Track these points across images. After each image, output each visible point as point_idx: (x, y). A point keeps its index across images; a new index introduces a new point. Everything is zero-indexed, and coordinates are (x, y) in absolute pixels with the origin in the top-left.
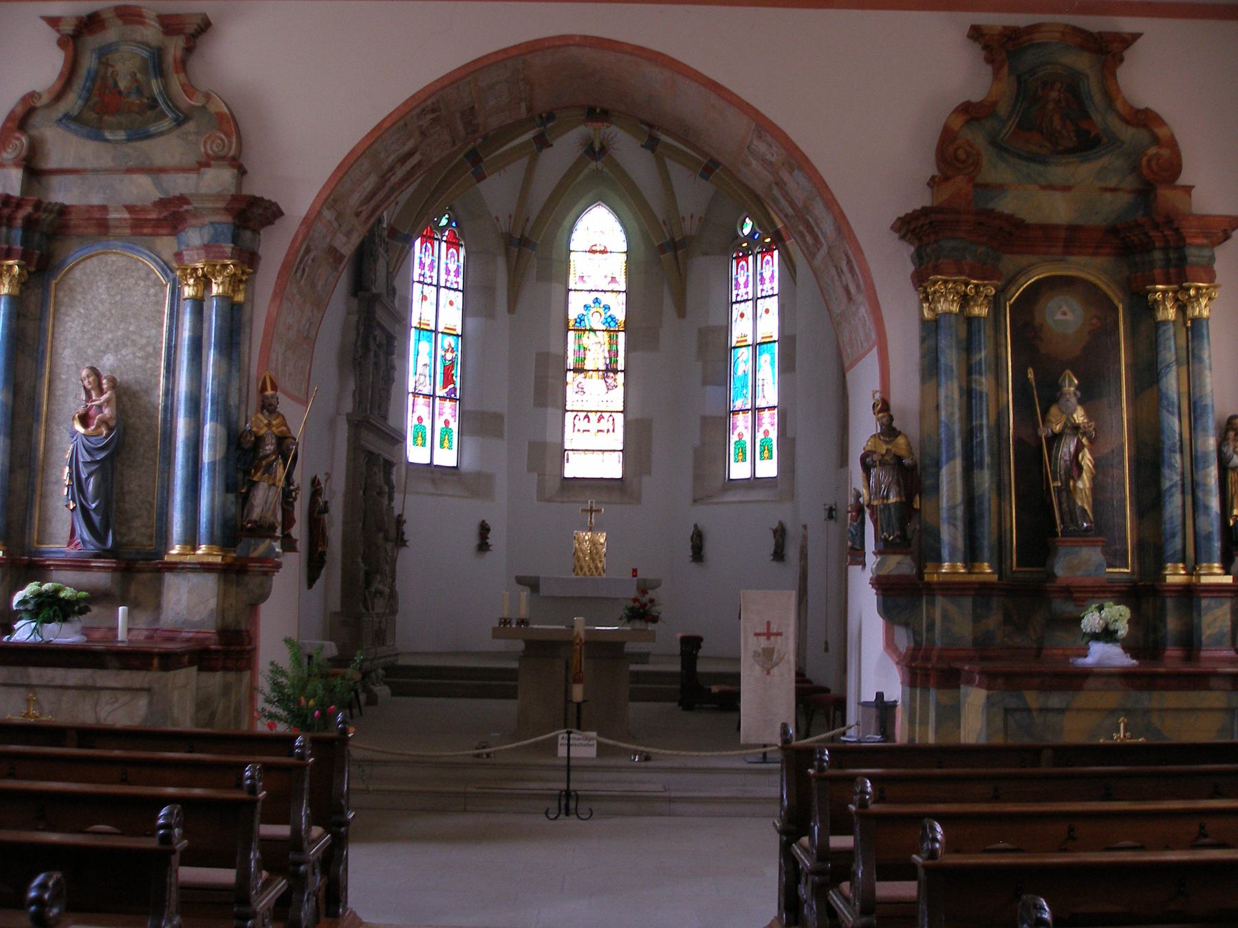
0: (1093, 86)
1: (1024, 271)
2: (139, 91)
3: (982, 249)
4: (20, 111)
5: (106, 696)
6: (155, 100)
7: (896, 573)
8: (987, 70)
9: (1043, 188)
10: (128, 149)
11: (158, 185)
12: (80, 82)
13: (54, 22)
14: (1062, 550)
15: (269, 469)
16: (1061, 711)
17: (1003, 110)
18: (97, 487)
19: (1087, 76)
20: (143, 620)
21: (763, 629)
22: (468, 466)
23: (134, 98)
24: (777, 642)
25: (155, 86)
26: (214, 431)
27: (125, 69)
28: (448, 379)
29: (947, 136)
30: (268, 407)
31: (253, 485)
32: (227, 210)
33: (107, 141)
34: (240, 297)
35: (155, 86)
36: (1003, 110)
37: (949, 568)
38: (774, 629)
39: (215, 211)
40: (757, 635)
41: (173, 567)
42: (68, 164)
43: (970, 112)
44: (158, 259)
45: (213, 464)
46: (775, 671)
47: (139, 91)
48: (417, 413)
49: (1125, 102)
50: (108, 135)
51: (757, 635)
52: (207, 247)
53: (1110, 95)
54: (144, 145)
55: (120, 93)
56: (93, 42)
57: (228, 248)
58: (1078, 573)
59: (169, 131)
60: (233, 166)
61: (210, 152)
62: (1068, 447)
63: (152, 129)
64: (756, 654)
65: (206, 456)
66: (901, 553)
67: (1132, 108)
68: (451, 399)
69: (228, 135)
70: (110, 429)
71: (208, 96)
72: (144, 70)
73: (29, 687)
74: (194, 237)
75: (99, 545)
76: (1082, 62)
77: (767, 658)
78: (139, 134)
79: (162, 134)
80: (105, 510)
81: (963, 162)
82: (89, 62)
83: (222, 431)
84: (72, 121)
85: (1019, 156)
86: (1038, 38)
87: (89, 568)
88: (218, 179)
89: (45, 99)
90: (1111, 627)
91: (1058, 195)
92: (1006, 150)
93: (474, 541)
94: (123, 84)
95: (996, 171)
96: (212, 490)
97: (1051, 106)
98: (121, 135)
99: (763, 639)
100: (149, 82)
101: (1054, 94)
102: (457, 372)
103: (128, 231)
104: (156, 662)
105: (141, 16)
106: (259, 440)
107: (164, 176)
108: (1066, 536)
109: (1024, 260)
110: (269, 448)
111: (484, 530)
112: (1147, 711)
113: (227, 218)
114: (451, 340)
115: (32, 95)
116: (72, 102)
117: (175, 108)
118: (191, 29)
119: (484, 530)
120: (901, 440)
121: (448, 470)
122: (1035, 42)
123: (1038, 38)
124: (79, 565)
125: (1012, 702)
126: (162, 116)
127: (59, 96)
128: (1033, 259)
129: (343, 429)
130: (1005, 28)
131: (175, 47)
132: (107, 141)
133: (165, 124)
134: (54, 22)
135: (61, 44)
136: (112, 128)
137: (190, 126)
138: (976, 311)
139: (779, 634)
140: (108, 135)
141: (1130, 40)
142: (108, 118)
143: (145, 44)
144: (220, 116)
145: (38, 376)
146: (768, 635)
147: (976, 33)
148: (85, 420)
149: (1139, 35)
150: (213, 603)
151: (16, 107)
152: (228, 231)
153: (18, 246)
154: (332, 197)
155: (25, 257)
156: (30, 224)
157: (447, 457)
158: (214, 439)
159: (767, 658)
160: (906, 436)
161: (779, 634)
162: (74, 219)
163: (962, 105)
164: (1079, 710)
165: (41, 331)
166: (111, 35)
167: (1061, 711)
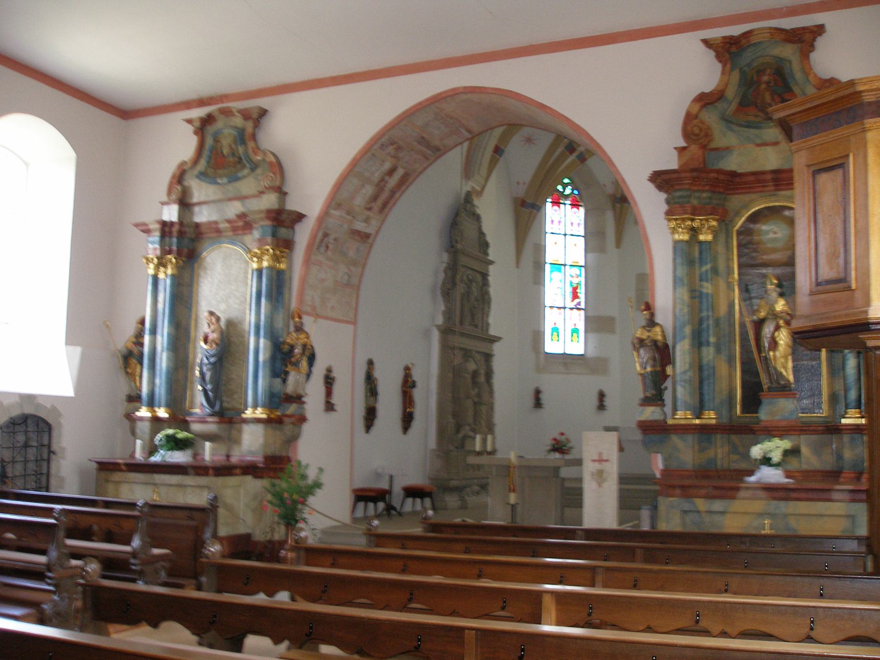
0: (796, 67)
1: (746, 207)
2: (233, 155)
3: (705, 195)
4: (178, 173)
5: (189, 490)
6: (240, 158)
7: (651, 418)
8: (719, 67)
9: (758, 145)
10: (230, 187)
11: (243, 205)
12: (206, 153)
13: (189, 121)
14: (765, 401)
15: (296, 364)
16: (722, 513)
17: (730, 93)
18: (212, 377)
19: (790, 62)
20: (222, 450)
21: (596, 457)
22: (591, 353)
23: (231, 159)
24: (605, 466)
25: (241, 149)
26: (265, 344)
27: (226, 143)
28: (575, 296)
29: (689, 118)
30: (299, 329)
31: (287, 373)
32: (268, 218)
33: (219, 184)
34: (283, 266)
35: (241, 149)
36: (730, 93)
37: (683, 416)
38: (605, 458)
39: (262, 219)
40: (594, 461)
41: (245, 421)
42: (203, 199)
43: (705, 100)
44: (243, 246)
45: (264, 362)
46: (605, 485)
47: (233, 155)
48: (551, 318)
49: (815, 76)
50: (219, 181)
51: (594, 461)
52: (259, 240)
53: (807, 70)
54: (238, 184)
55: (224, 156)
56: (211, 129)
57: (269, 239)
58: (777, 418)
59: (248, 175)
60: (276, 191)
61: (266, 185)
62: (767, 330)
63: (240, 174)
64: (593, 474)
65: (261, 358)
66: (653, 405)
67: (820, 79)
68: (579, 309)
69: (274, 174)
70: (217, 344)
71: (265, 154)
72: (235, 142)
73: (155, 484)
74: (256, 234)
75: (211, 409)
76: (788, 52)
77: (600, 476)
78: (234, 179)
79: (245, 177)
80: (216, 390)
81: (697, 135)
82: (209, 141)
83: (269, 343)
84: (203, 176)
85: (741, 126)
86: (754, 40)
87: (206, 422)
88: (269, 201)
89: (189, 165)
90: (768, 456)
91: (769, 149)
92: (732, 123)
93: (595, 402)
94: (225, 151)
95: (723, 137)
96: (264, 377)
97: (763, 86)
98: (225, 180)
99: (597, 464)
100: (237, 149)
101: (765, 78)
102: (581, 292)
103: (230, 233)
104: (211, 471)
105: (232, 112)
106: (292, 347)
107: (247, 201)
108: (771, 391)
109: (746, 198)
110: (297, 351)
111: (602, 396)
112: (786, 516)
113: (268, 223)
114: (576, 271)
115: (184, 163)
116: (202, 164)
117: (251, 161)
118: (255, 116)
119: (602, 396)
120: (657, 329)
121: (578, 356)
122: (752, 42)
123: (754, 40)
124: (202, 421)
125: (686, 506)
126: (244, 167)
127: (196, 161)
128: (753, 196)
129: (436, 335)
130: (724, 38)
131: (249, 126)
132: (219, 184)
133: (246, 172)
134: (189, 121)
135: (196, 133)
136: (221, 177)
137: (259, 171)
138: (702, 238)
139: (607, 461)
140: (219, 181)
141: (819, 30)
142: (220, 172)
143: (236, 128)
144: (271, 164)
145: (190, 317)
146: (600, 461)
147: (706, 42)
148: (206, 341)
149: (183, 120)
150: (261, 440)
151: (690, 106)
152: (269, 230)
153: (174, 248)
154: (335, 201)
155: (179, 254)
156: (181, 234)
157: (577, 348)
158: (265, 348)
159: (600, 476)
160: (661, 326)
161: (607, 461)
162: (203, 229)
163: (698, 96)
164: (734, 513)
165: (191, 292)
166: (219, 124)
167: (722, 513)
